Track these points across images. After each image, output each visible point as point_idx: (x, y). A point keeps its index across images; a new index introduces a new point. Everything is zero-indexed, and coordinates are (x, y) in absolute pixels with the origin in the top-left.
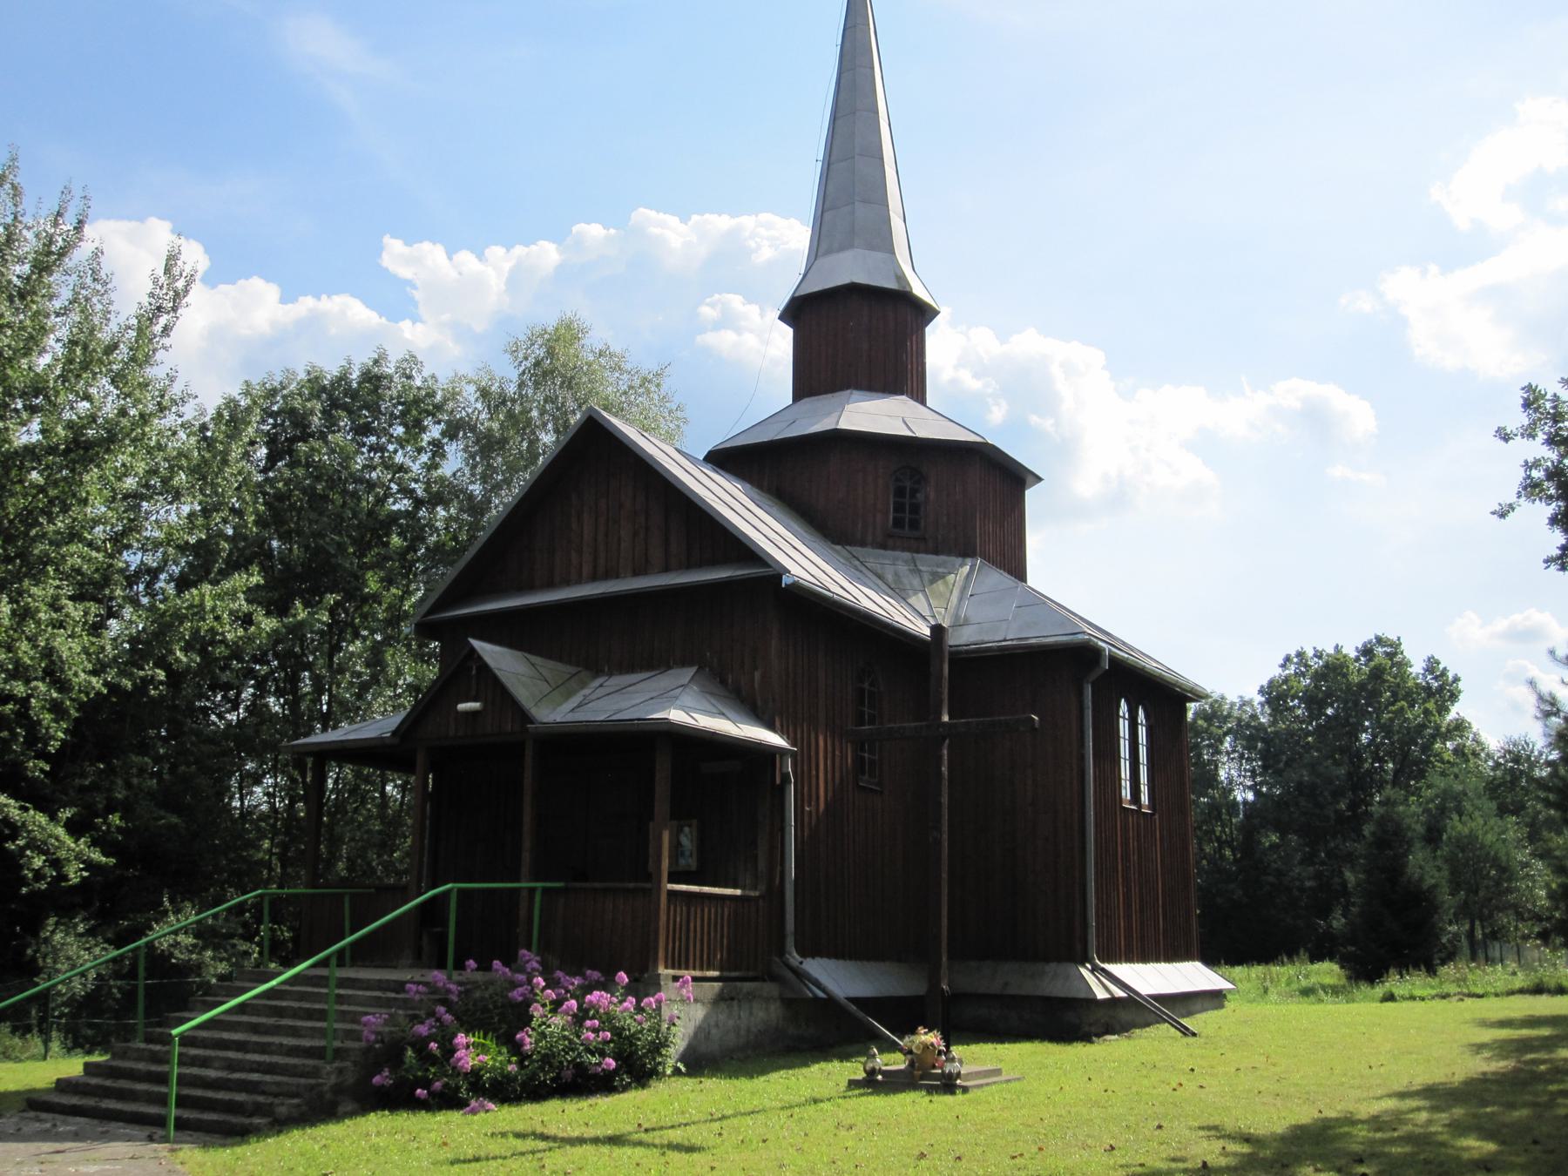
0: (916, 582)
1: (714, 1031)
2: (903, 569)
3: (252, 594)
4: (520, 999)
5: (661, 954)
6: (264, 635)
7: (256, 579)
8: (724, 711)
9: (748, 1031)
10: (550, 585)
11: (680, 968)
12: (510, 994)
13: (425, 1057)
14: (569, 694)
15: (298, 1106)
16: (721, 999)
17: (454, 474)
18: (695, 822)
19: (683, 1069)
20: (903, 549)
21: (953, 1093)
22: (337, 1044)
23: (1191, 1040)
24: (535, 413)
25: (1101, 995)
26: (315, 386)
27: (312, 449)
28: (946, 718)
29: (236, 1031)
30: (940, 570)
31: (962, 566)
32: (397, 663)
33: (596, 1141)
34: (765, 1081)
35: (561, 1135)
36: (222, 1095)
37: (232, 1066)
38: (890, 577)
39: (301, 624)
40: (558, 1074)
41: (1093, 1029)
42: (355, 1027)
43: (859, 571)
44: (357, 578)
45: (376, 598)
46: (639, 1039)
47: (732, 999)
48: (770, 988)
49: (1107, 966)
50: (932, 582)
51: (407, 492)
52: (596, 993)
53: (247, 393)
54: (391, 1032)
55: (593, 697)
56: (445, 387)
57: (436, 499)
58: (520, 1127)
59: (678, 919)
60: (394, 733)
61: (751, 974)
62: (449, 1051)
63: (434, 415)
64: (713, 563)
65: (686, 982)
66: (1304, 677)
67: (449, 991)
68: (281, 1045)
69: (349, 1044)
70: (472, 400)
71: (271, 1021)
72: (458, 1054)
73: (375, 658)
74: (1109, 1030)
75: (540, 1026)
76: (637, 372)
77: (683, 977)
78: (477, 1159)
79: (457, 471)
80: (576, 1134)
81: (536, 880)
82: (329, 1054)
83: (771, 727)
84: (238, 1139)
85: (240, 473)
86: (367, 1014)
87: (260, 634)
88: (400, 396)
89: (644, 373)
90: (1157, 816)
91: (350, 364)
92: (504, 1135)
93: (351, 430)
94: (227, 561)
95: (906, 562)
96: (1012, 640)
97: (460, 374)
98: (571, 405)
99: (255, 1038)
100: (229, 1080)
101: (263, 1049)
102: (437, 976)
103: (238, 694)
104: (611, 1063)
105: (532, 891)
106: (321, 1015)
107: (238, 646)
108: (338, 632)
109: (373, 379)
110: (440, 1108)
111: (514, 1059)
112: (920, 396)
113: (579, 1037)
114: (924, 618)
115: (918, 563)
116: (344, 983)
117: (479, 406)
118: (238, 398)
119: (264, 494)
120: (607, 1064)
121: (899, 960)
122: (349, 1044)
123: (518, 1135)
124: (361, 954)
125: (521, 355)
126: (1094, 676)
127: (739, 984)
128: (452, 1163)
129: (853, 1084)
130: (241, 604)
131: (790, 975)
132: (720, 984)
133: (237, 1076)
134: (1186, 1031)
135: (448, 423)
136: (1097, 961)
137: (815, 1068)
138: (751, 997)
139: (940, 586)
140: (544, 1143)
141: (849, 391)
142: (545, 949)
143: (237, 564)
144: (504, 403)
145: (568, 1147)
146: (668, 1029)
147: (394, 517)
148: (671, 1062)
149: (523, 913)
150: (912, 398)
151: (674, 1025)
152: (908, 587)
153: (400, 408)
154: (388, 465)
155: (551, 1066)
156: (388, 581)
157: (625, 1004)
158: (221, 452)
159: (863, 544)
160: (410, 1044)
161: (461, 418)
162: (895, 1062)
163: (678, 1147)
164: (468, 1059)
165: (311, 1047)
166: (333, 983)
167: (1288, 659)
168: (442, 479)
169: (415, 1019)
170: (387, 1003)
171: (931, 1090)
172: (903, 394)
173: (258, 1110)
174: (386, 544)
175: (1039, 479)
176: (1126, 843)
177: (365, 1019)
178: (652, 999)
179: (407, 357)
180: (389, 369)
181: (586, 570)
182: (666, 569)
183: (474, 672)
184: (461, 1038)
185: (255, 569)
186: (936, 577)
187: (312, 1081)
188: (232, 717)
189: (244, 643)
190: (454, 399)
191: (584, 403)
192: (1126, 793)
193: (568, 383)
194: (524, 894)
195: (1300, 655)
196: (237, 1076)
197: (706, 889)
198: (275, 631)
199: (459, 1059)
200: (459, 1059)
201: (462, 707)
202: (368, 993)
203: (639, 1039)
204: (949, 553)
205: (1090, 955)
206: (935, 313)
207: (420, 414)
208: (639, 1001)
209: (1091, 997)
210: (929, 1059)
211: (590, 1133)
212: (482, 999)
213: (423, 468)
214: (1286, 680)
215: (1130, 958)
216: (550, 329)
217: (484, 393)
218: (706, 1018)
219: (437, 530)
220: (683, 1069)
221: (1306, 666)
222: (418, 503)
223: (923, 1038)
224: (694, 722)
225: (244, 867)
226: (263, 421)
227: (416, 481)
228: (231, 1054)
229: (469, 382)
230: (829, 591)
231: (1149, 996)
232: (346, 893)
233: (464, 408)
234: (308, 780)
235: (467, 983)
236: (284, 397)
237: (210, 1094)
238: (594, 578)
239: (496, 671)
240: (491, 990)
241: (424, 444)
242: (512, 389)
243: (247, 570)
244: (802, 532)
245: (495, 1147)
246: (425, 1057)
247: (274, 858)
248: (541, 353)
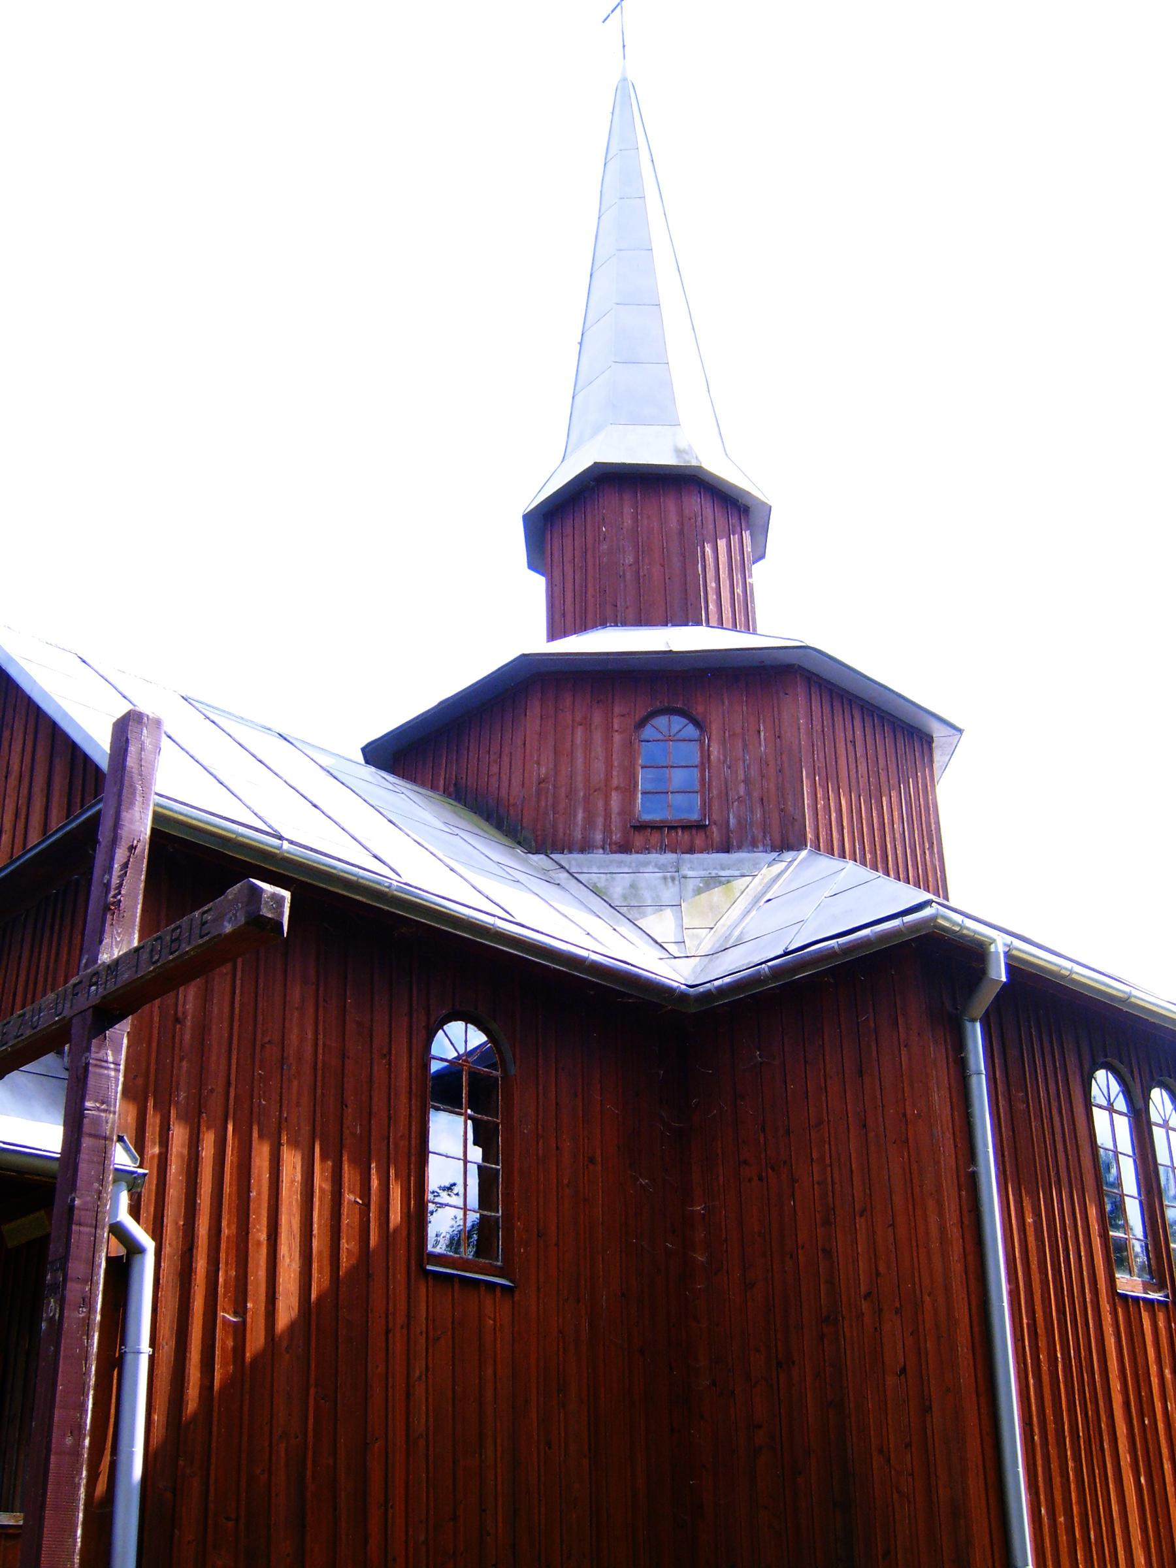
95: (662, 868)
126: (985, 998)
139: (716, 894)
159: (585, 847)
186: (712, 882)
230: (281, 838)
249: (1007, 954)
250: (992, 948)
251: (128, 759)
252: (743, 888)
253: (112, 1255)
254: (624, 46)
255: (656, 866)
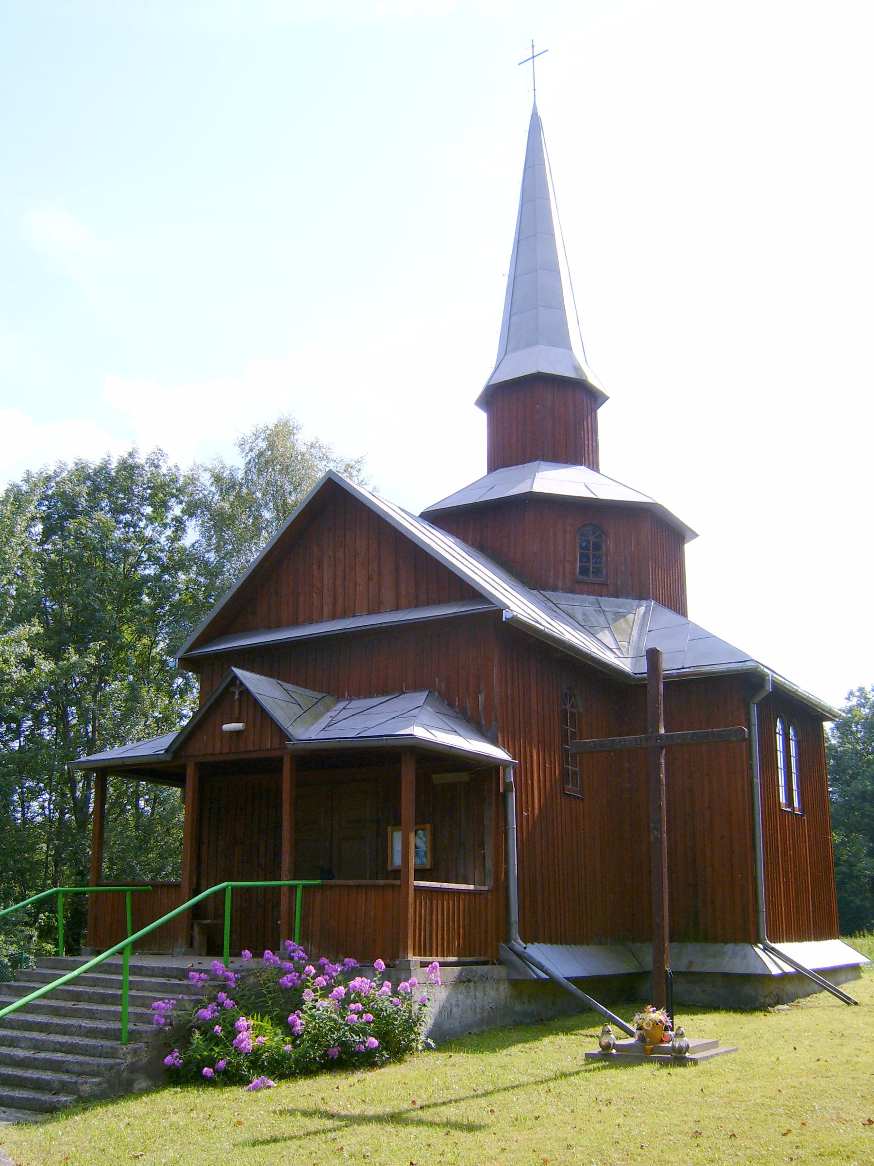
0: (602, 620)
1: (455, 1010)
2: (590, 610)
3: (33, 641)
4: (290, 984)
5: (410, 943)
6: (44, 674)
7: (38, 629)
8: (456, 730)
9: (483, 1008)
10: (295, 623)
11: (425, 955)
12: (281, 980)
13: (212, 1040)
14: (318, 716)
15: (100, 1084)
16: (461, 981)
17: (193, 545)
18: (428, 826)
19: (433, 1044)
20: (589, 594)
21: (684, 1065)
22: (131, 1026)
23: (853, 1008)
24: (259, 495)
25: (775, 971)
26: (82, 474)
27: (81, 524)
28: (662, 731)
29: (38, 1014)
30: (620, 610)
31: (638, 606)
32: (151, 698)
33: (379, 1119)
34: (507, 1055)
35: (343, 1113)
36: (30, 1074)
37: (38, 1046)
38: (579, 617)
39: (74, 665)
40: (325, 1051)
41: (768, 1001)
42: (145, 1010)
43: (555, 611)
44: (115, 628)
45: (131, 646)
46: (396, 1019)
47: (469, 981)
48: (498, 971)
49: (777, 946)
50: (615, 620)
51: (156, 560)
52: (358, 979)
53: (27, 481)
54: (179, 1016)
55: (340, 717)
56: (186, 474)
57: (181, 566)
58: (303, 1104)
59: (423, 912)
60: (167, 751)
61: (483, 958)
62: (232, 1033)
63: (177, 497)
64: (439, 601)
65: (434, 968)
66: (864, 707)
67: (227, 978)
68: (80, 1026)
69: (141, 1027)
70: (208, 484)
71: (70, 1004)
72: (240, 1036)
73: (134, 696)
74: (779, 1001)
75: (310, 1009)
76: (341, 461)
77: (431, 963)
78: (275, 1140)
79: (196, 542)
80: (357, 1111)
81: (295, 879)
82: (125, 1036)
83: (494, 742)
84: (48, 1116)
85: (23, 544)
86: (156, 999)
87: (40, 674)
88: (149, 481)
89: (347, 461)
90: (805, 817)
91: (109, 457)
92: (292, 1112)
93: (110, 510)
94: (12, 615)
95: (592, 604)
96: (690, 667)
97: (198, 464)
98: (288, 487)
99: (56, 1020)
100: (35, 1059)
101: (64, 1030)
102: (215, 963)
103: (19, 726)
104: (374, 1042)
105: (292, 889)
106: (115, 1000)
107: (23, 685)
108: (101, 673)
109: (128, 469)
110: (226, 1085)
111: (288, 1039)
112: (594, 466)
113: (343, 1018)
114: (611, 650)
115: (602, 605)
116: (136, 970)
117: (213, 489)
118: (21, 483)
119: (43, 561)
120: (371, 1043)
121: (600, 943)
122: (141, 1027)
123: (305, 1114)
124: (138, 946)
125: (247, 448)
126: (759, 698)
127: (474, 967)
128: (254, 1145)
129: (590, 1058)
130: (25, 649)
131: (516, 959)
132: (460, 968)
133: (43, 1055)
134: (848, 1001)
135: (189, 504)
136: (768, 941)
137: (546, 1040)
138: (484, 978)
139: (621, 623)
140: (330, 1121)
141: (537, 462)
142: (305, 938)
143: (20, 618)
144: (233, 487)
145: (356, 1126)
146: (420, 1009)
147: (146, 579)
148: (422, 1038)
149: (284, 907)
150: (589, 467)
151: (424, 1005)
152: (596, 624)
153: (149, 491)
154: (140, 538)
155: (320, 1045)
156: (141, 632)
157: (383, 989)
158: (8, 525)
159: (555, 589)
160: (199, 1028)
161: (199, 499)
162: (616, 1036)
163: (458, 1126)
164: (248, 1040)
165: (108, 1029)
166: (126, 970)
167: (851, 694)
168: (183, 550)
169: (198, 1003)
170: (173, 989)
171: (664, 1063)
172: (581, 465)
173: (64, 1088)
174: (139, 602)
175: (696, 535)
176: (784, 839)
177: (156, 1004)
178: (407, 984)
179: (156, 451)
180: (141, 459)
181: (327, 610)
182: (397, 608)
183: (237, 697)
184: (242, 1022)
185: (35, 620)
186: (618, 616)
187: (111, 1061)
188: (16, 745)
189: (27, 682)
190: (194, 483)
191: (299, 486)
192: (782, 799)
193: (286, 470)
194: (285, 890)
195: (861, 690)
196: (43, 1055)
197: (446, 885)
198: (52, 672)
199: (242, 1041)
200: (242, 1041)
201: (226, 727)
202: (154, 980)
203: (396, 1019)
204: (627, 597)
205: (762, 936)
206: (608, 398)
207: (165, 496)
208: (395, 986)
209: (767, 973)
210: (658, 1033)
211: (371, 1110)
212: (257, 984)
213: (168, 540)
214: (850, 710)
215: (790, 940)
216: (271, 426)
217: (217, 479)
218: (448, 998)
219: (179, 590)
220: (433, 1044)
221: (865, 698)
222: (165, 569)
223: (653, 1016)
224: (434, 738)
225: (27, 866)
226: (40, 504)
227: (162, 551)
228: (35, 1035)
229: (205, 470)
231: (813, 970)
232: (128, 891)
233: (201, 491)
234: (78, 794)
235: (242, 971)
236: (57, 483)
237: (19, 1072)
238: (333, 617)
239: (256, 695)
240: (265, 976)
241: (168, 521)
242: (240, 475)
243: (30, 621)
244: (508, 580)
245: (287, 1126)
246: (212, 1040)
247: (50, 858)
248: (263, 445)
249: (772, 680)
250: (767, 678)
251: (617, 1027)
252: (632, 620)
253: (282, 888)
254: (535, 90)
255: (589, 603)
